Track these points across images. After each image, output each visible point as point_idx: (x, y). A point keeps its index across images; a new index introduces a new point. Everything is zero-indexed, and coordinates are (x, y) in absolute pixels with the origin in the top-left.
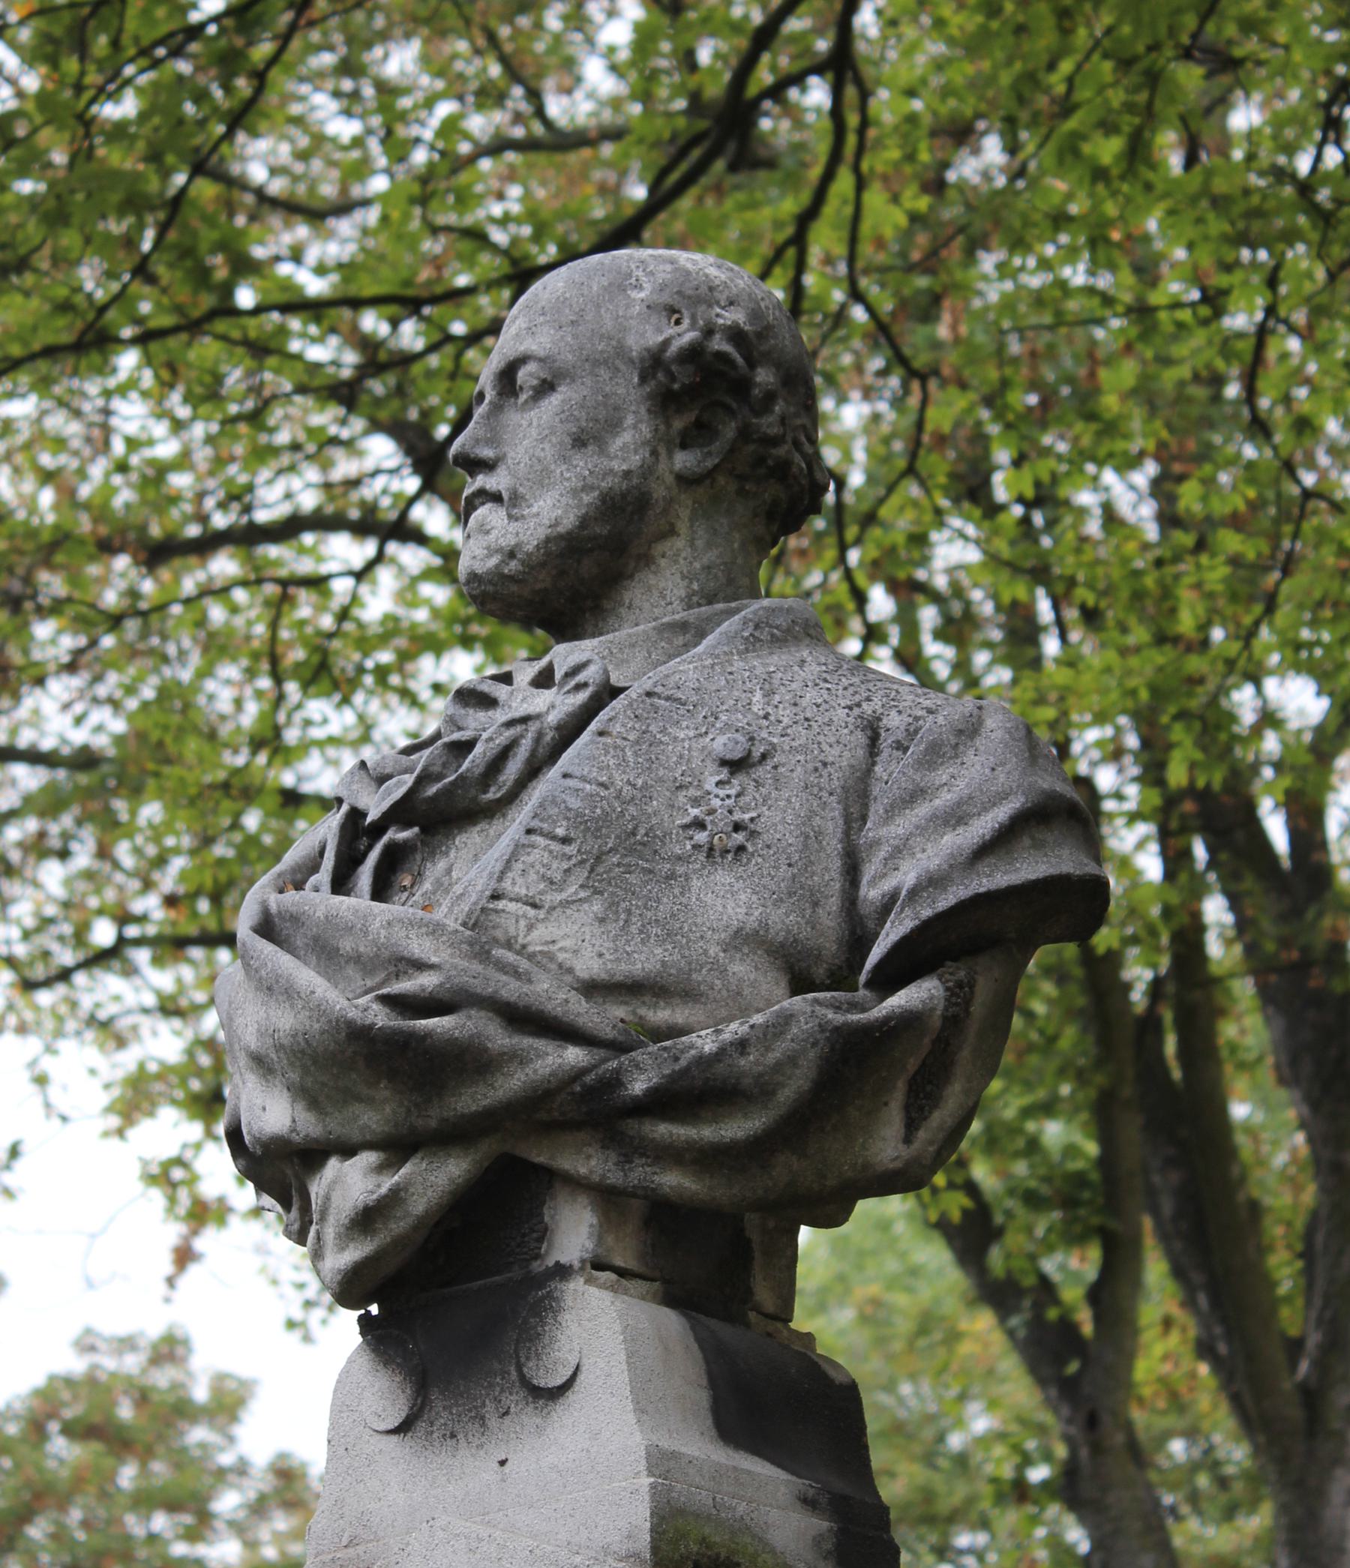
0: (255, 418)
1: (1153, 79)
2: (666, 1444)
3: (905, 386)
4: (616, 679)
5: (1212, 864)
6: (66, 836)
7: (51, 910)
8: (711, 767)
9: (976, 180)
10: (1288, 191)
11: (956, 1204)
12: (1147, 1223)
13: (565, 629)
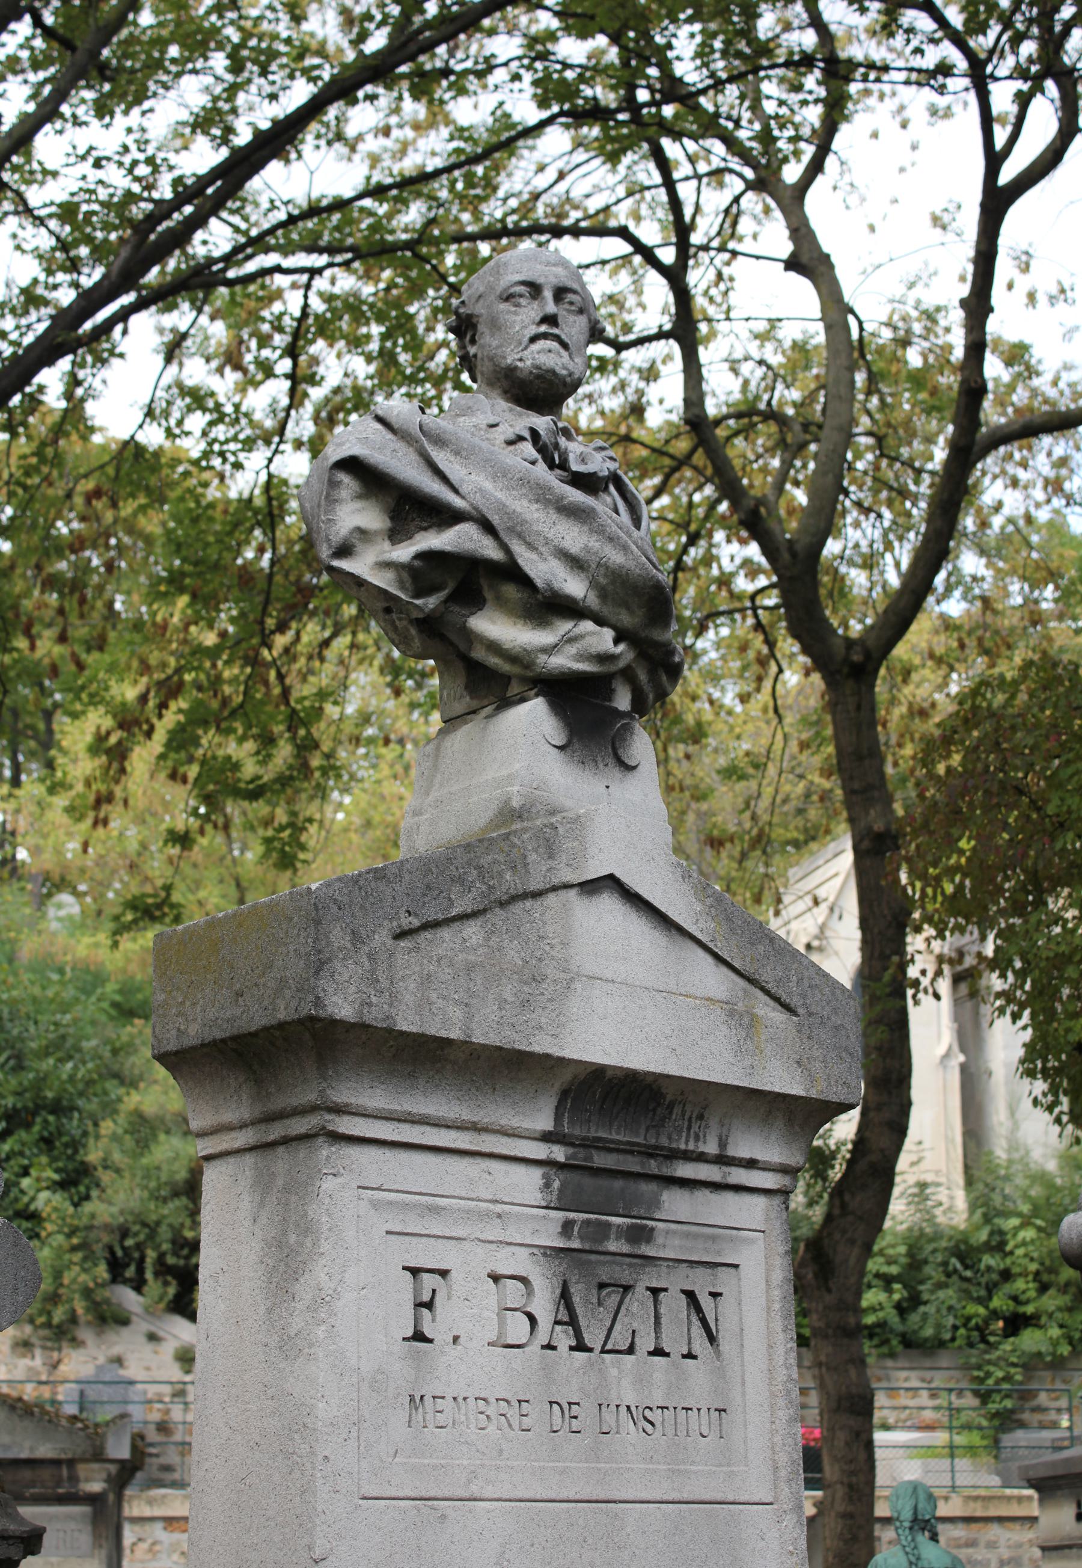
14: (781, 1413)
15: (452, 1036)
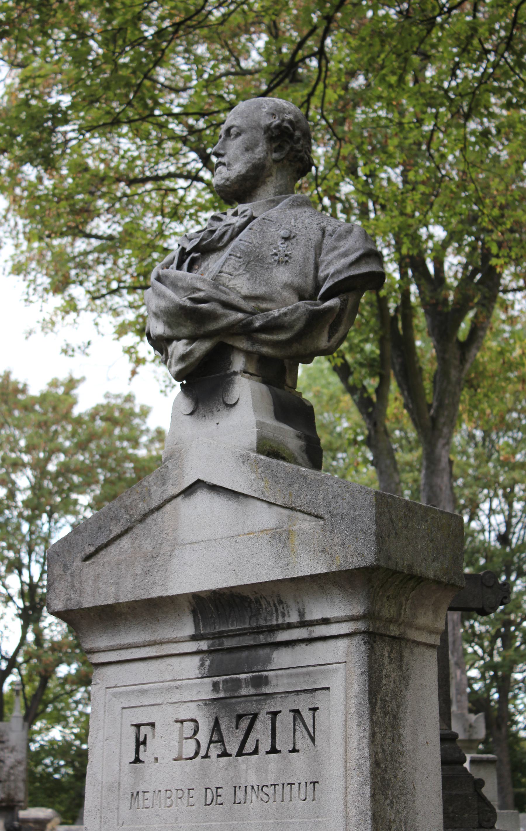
0: (159, 145)
1: (406, 60)
2: (261, 420)
3: (335, 144)
4: (255, 214)
5: (413, 276)
6: (105, 259)
7: (101, 278)
8: (280, 239)
9: (357, 88)
10: (442, 92)
11: (339, 361)
12: (392, 372)
13: (242, 201)
14: (353, 781)
15: (110, 602)
